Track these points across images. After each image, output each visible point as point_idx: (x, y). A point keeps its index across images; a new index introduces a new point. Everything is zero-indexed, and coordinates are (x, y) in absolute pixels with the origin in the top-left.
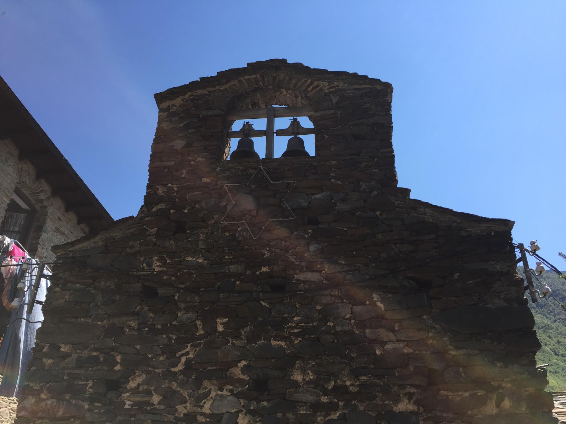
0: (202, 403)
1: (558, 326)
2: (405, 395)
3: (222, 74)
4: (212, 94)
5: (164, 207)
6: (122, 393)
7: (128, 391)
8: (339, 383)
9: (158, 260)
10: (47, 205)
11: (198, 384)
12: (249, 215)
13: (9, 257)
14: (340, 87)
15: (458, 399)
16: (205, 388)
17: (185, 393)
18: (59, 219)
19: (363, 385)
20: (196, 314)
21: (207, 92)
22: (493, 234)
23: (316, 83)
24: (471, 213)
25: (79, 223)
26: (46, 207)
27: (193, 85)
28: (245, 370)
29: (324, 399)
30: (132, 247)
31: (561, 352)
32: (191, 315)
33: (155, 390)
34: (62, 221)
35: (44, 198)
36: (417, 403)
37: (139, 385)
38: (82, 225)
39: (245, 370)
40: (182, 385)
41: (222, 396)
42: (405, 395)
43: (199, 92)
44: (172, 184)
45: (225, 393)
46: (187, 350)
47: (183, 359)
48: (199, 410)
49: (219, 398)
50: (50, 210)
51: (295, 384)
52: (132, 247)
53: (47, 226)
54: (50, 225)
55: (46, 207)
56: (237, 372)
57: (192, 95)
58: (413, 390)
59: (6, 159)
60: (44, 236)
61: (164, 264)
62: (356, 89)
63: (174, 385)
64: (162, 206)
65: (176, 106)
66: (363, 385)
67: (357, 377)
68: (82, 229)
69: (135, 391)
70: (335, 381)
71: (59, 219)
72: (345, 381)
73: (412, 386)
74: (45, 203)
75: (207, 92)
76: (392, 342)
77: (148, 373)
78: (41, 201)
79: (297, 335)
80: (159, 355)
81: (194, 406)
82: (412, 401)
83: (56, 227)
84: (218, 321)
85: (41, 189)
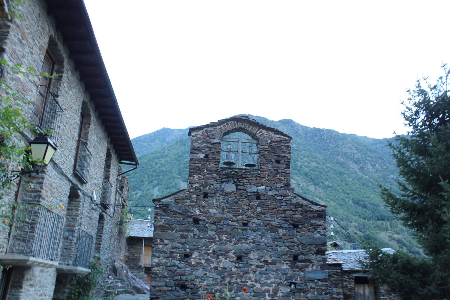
0: (219, 264)
1: (349, 173)
3: (219, 121)
4: (215, 130)
5: (198, 185)
6: (190, 259)
7: (193, 258)
8: (265, 259)
9: (198, 209)
11: (217, 257)
15: (301, 265)
17: (213, 260)
19: (273, 260)
21: (213, 129)
23: (261, 130)
27: (208, 126)
28: (234, 253)
29: (260, 264)
30: (186, 202)
31: (347, 192)
37: (196, 256)
39: (234, 253)
40: (212, 257)
43: (209, 129)
44: (201, 175)
46: (213, 245)
47: (212, 249)
48: (218, 266)
51: (251, 259)
52: (186, 202)
57: (206, 130)
58: (288, 262)
61: (201, 211)
62: (278, 138)
63: (209, 257)
64: (197, 185)
65: (199, 135)
67: (271, 257)
69: (195, 258)
73: (289, 261)
75: (213, 129)
76: (283, 246)
77: (199, 252)
79: (252, 243)
80: (203, 247)
84: (224, 236)
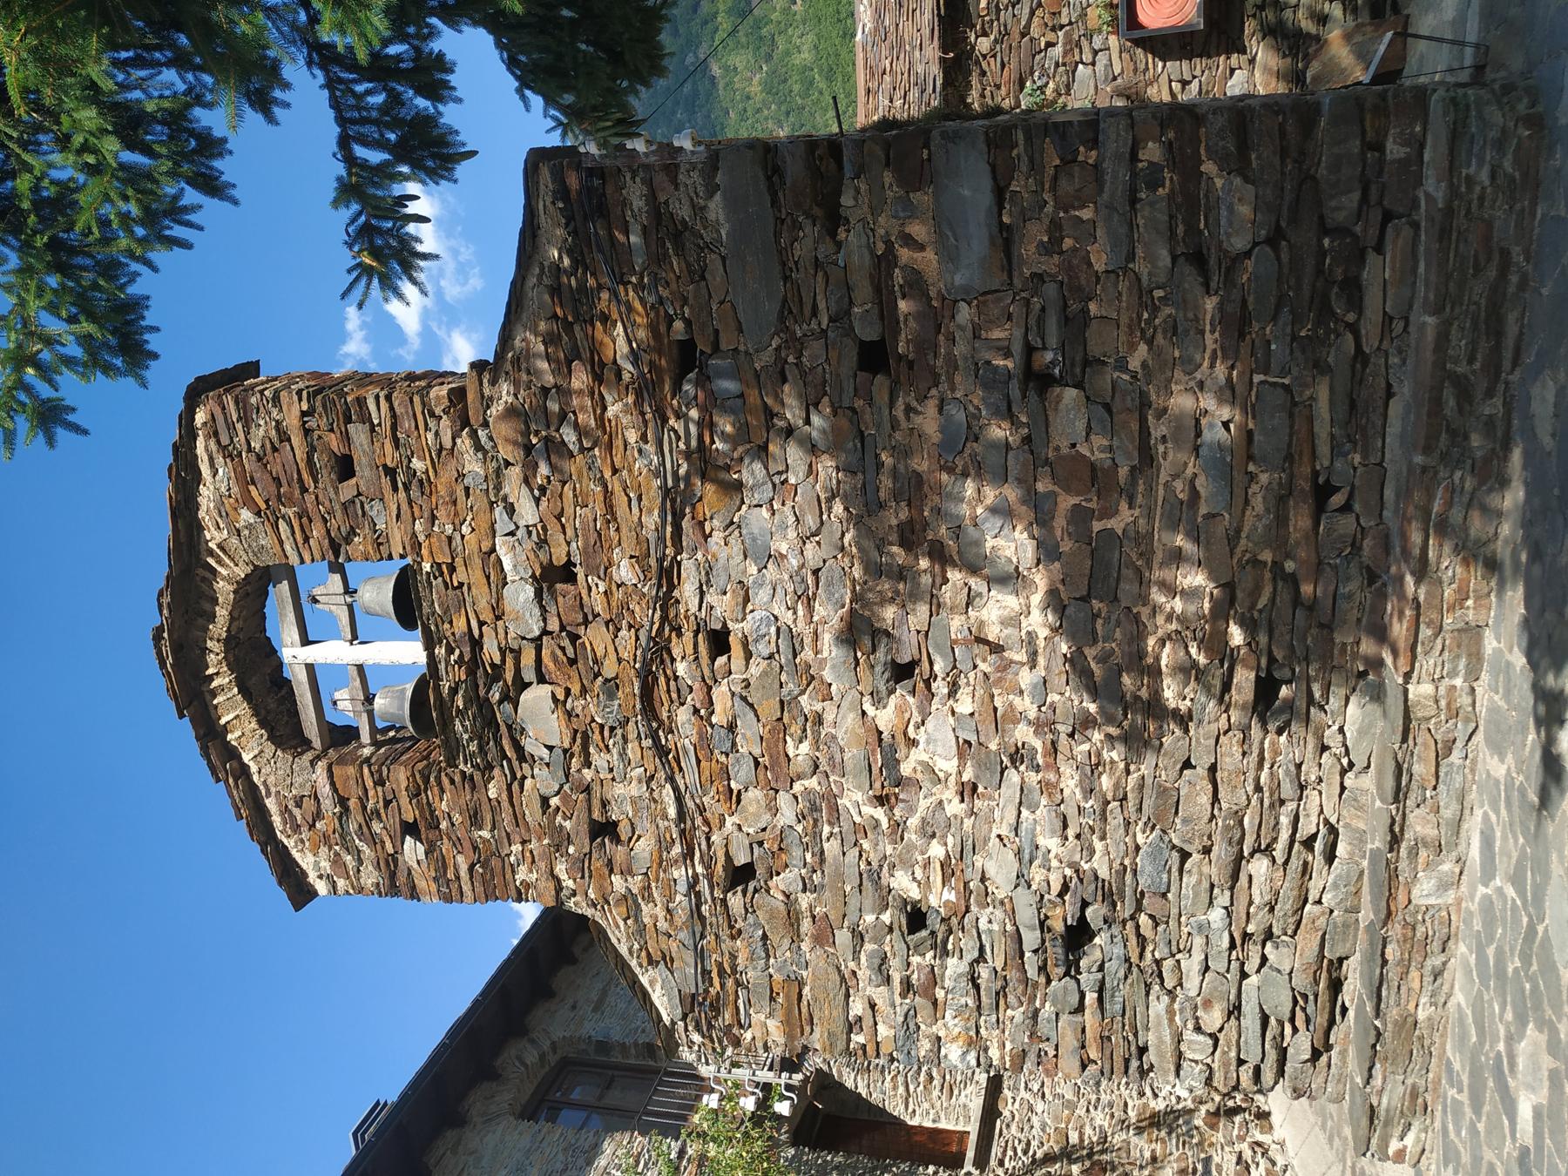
2: (908, 419)
10: (548, 1043)
12: (565, 702)
13: (74, 310)
14: (212, 505)
15: (912, 324)
16: (915, 770)
17: (924, 804)
18: (574, 1007)
20: (781, 793)
22: (561, 205)
24: (516, 245)
25: (573, 961)
26: (553, 1043)
32: (783, 799)
33: (923, 853)
34: (576, 1002)
35: (535, 1053)
36: (923, 398)
38: (577, 951)
40: (912, 810)
41: (928, 742)
42: (908, 419)
45: (921, 737)
46: (848, 805)
48: (952, 780)
49: (931, 746)
50: (558, 1033)
53: (593, 1033)
54: (593, 1027)
55: (553, 1043)
56: (885, 718)
59: (471, 1154)
60: (616, 1035)
63: (913, 822)
66: (896, 495)
68: (585, 950)
69: (925, 885)
70: (891, 544)
71: (574, 1007)
72: (890, 526)
74: (546, 1045)
78: (542, 1057)
81: (946, 786)
82: (920, 409)
83: (593, 1011)
85: (517, 1064)
